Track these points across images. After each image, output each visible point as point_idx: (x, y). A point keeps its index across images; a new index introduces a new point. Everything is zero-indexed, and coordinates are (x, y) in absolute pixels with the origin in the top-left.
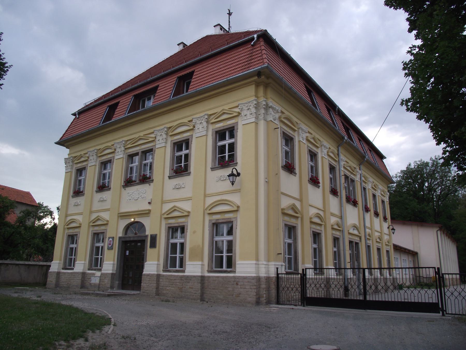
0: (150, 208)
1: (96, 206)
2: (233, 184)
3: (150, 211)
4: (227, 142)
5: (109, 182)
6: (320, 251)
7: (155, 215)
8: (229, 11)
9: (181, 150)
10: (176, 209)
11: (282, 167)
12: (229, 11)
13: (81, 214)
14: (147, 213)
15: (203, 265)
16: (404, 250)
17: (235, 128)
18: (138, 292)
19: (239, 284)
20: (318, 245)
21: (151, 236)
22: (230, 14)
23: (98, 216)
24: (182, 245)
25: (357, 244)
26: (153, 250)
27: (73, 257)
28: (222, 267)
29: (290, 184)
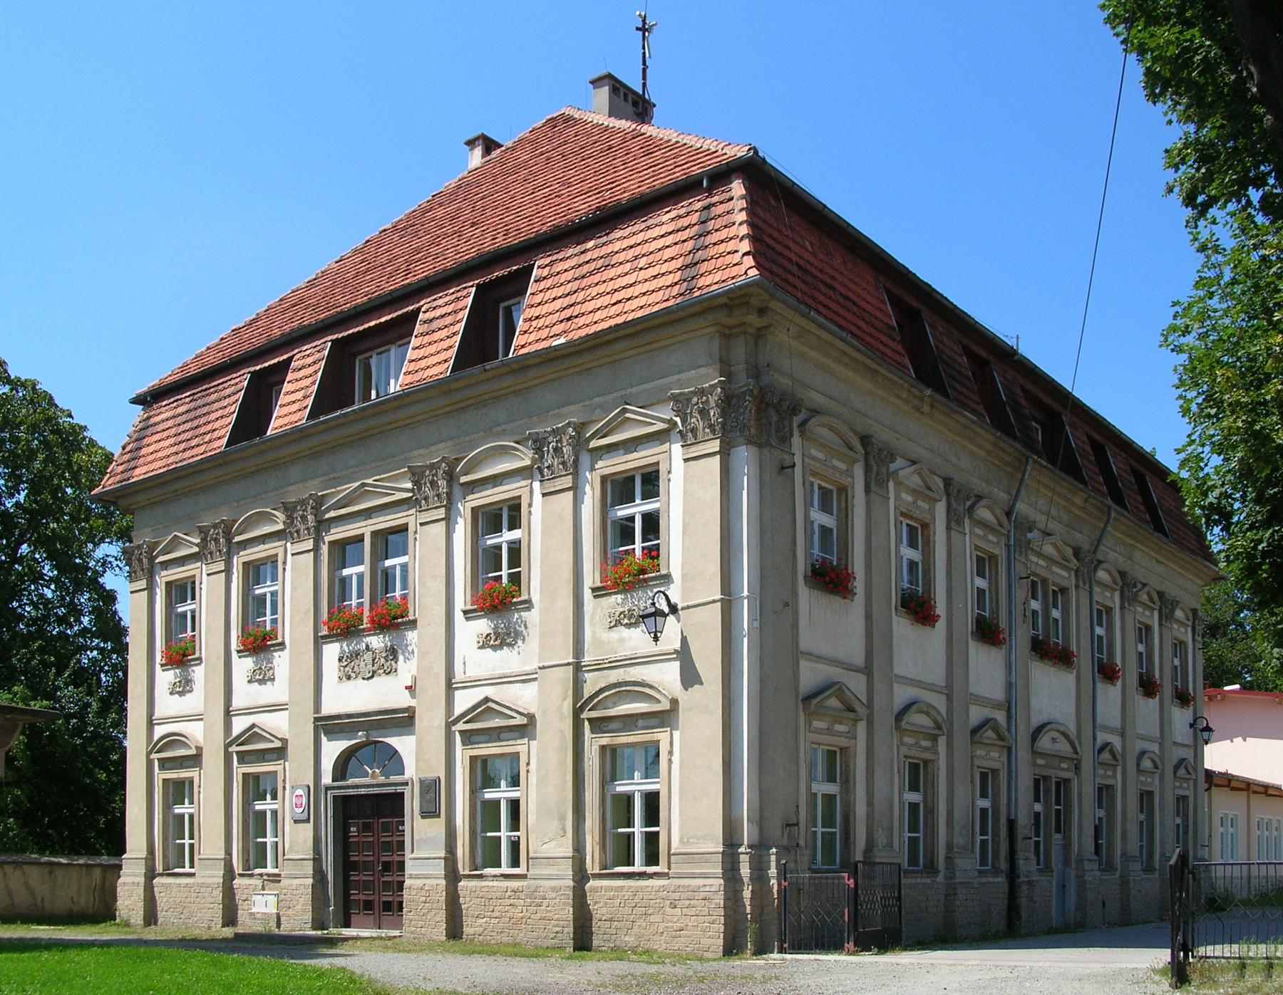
0: (413, 703)
1: (245, 693)
2: (656, 639)
3: (411, 712)
4: (637, 509)
5: (274, 621)
6: (931, 811)
7: (431, 720)
8: (644, 21)
9: (498, 529)
10: (490, 704)
11: (806, 577)
12: (644, 21)
13: (198, 718)
14: (403, 720)
15: (1078, 678)
16: (1261, 789)
17: (663, 468)
18: (396, 933)
19: (680, 904)
20: (925, 796)
21: (422, 782)
22: (644, 29)
23: (253, 726)
24: (515, 805)
25: (1063, 784)
26: (431, 775)
27: (187, 841)
28: (630, 862)
29: (832, 629)
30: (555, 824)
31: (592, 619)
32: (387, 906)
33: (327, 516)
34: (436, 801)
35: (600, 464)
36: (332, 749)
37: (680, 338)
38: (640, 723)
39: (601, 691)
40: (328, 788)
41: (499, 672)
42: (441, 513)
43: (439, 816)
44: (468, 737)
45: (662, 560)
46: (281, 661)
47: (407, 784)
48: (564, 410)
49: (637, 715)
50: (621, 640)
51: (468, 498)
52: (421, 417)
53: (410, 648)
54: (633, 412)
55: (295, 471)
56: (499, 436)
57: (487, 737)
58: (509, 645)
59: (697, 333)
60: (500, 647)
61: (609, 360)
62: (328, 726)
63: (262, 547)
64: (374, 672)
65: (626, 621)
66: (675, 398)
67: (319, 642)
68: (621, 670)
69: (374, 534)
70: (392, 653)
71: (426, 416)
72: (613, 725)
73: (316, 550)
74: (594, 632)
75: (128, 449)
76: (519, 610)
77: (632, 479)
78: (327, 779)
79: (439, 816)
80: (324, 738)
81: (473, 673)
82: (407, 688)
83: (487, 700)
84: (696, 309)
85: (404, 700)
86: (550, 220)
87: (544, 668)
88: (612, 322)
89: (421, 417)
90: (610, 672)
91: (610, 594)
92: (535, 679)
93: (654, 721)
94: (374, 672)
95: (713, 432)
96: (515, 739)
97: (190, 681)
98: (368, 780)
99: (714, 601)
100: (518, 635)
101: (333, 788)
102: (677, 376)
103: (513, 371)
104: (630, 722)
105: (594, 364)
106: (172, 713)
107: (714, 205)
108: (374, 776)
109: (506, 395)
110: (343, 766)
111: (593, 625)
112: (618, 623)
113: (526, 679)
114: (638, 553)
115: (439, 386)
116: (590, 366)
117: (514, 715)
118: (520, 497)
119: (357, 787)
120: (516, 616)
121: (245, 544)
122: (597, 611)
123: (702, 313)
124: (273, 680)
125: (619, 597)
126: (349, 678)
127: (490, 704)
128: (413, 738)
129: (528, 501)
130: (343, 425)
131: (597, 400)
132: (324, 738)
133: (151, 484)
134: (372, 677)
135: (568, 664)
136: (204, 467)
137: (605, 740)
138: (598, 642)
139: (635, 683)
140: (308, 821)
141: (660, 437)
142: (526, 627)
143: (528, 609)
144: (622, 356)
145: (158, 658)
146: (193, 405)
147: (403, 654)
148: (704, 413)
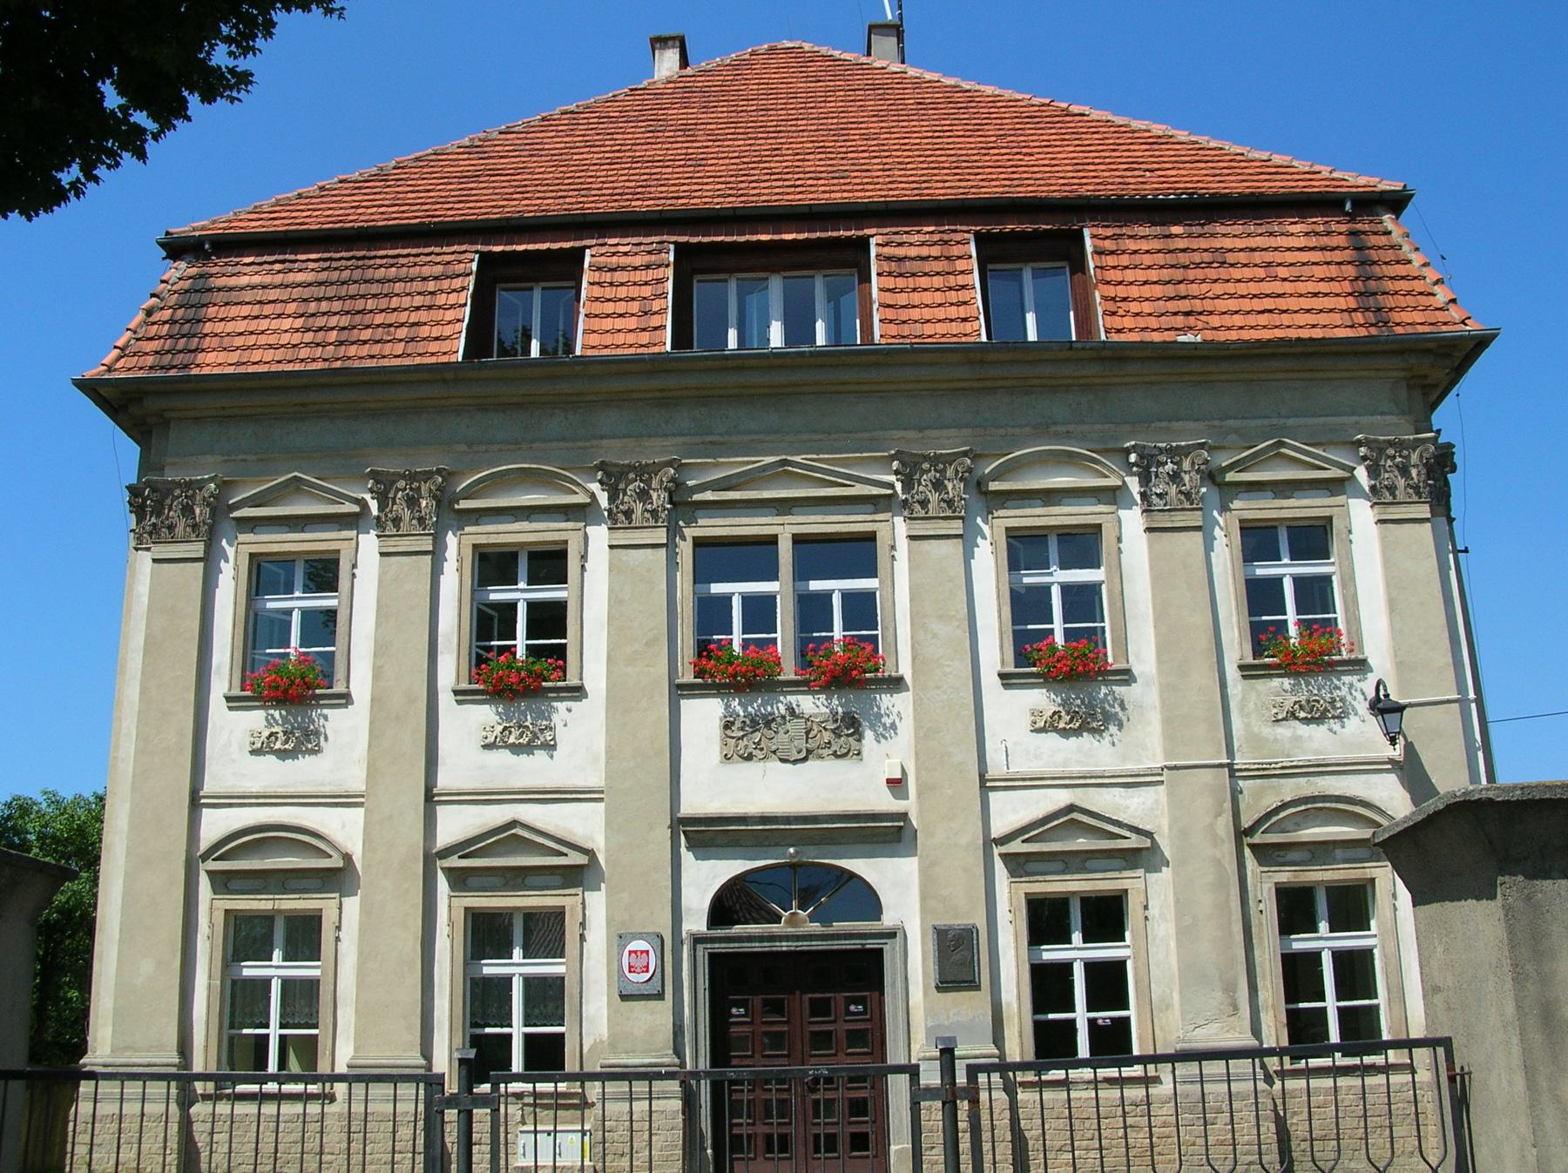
7: (948, 832)
10: (1075, 815)
14: (888, 834)
26: (959, 921)
30: (1216, 998)
31: (1242, 707)
32: (859, 1141)
33: (697, 497)
34: (970, 963)
35: (1236, 504)
36: (706, 878)
37: (1357, 374)
38: (1339, 853)
39: (1285, 806)
40: (697, 940)
41: (1076, 769)
42: (197, 549)
43: (978, 988)
44: (460, 880)
45: (339, 674)
46: (346, 730)
47: (892, 935)
48: (1176, 425)
49: (1335, 842)
50: (1297, 739)
51: (468, 529)
52: (910, 386)
53: (887, 721)
54: (1294, 447)
55: (608, 419)
56: (1067, 436)
57: (1060, 866)
58: (1093, 731)
59: (1381, 374)
60: (1077, 732)
61: (1247, 376)
62: (707, 834)
63: (525, 525)
64: (809, 752)
65: (1302, 715)
66: (374, 475)
67: (680, 691)
68: (1302, 780)
69: (798, 540)
70: (851, 725)
71: (919, 386)
72: (1293, 855)
73: (670, 546)
74: (1248, 725)
75: (156, 317)
76: (1106, 683)
77: (514, 556)
78: (696, 921)
79: (978, 988)
80: (687, 857)
81: (1020, 767)
82: (889, 781)
83: (1071, 808)
84: (1395, 346)
85: (885, 802)
86: (903, 191)
87: (1176, 768)
88: (1279, 333)
89: (910, 386)
90: (1282, 781)
91: (1271, 676)
92: (601, 800)
93: (258, 883)
94: (809, 752)
95: (1419, 494)
96: (1120, 870)
97: (317, 733)
98: (795, 927)
99: (1449, 701)
100: (1108, 718)
101: (712, 940)
102: (1356, 418)
103: (1103, 359)
104: (1322, 851)
105: (1223, 377)
106: (256, 788)
107: (211, 276)
108: (793, 921)
109: (1068, 386)
110: (725, 908)
111: (1244, 714)
112: (1292, 715)
113: (1133, 782)
114: (521, 653)
115: (441, 373)
116: (1214, 377)
117: (1127, 834)
118: (566, 542)
119: (750, 939)
120: (1104, 690)
121: (478, 516)
122: (704, 717)
123: (1401, 352)
124: (554, 747)
125: (1287, 683)
126: (749, 758)
127: (1075, 815)
128: (915, 859)
129: (1115, 534)
130: (752, 368)
131: (1231, 422)
132: (687, 857)
133: (248, 384)
134: (805, 759)
135: (1221, 766)
136: (399, 378)
137: (1285, 876)
138: (1256, 741)
139: (1339, 799)
140: (660, 996)
141: (351, 521)
142: (1123, 708)
143: (1127, 683)
144: (1271, 376)
145: (220, 685)
146: (323, 276)
147: (872, 727)
148: (412, 502)
